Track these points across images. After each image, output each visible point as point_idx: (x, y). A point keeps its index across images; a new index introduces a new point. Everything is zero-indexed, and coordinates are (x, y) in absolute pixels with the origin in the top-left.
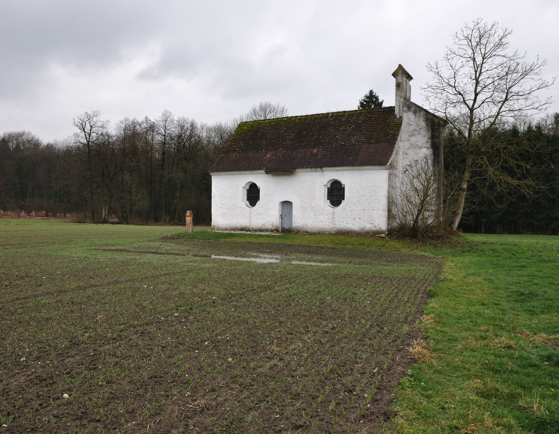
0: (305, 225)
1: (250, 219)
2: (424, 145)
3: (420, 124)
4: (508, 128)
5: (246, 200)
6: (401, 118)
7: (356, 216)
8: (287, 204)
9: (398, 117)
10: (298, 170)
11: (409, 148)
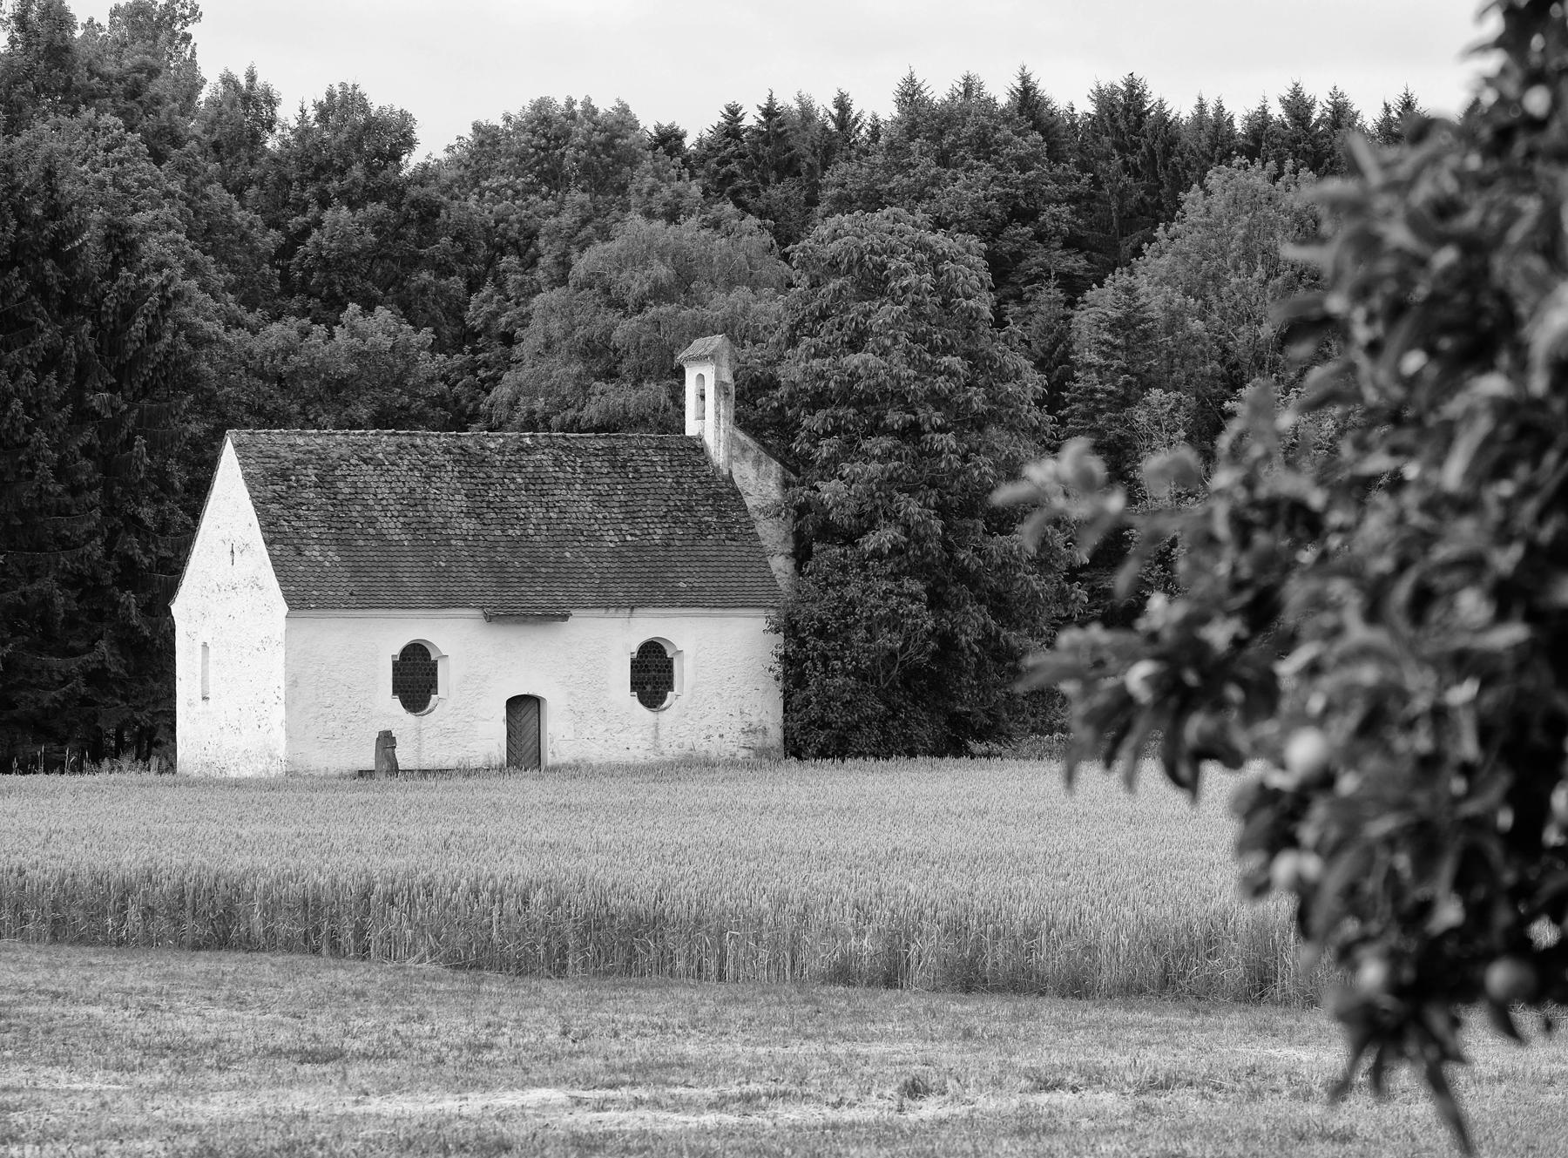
1: (419, 750)
2: (779, 548)
3: (1425, 908)
7: (711, 732)
8: (523, 709)
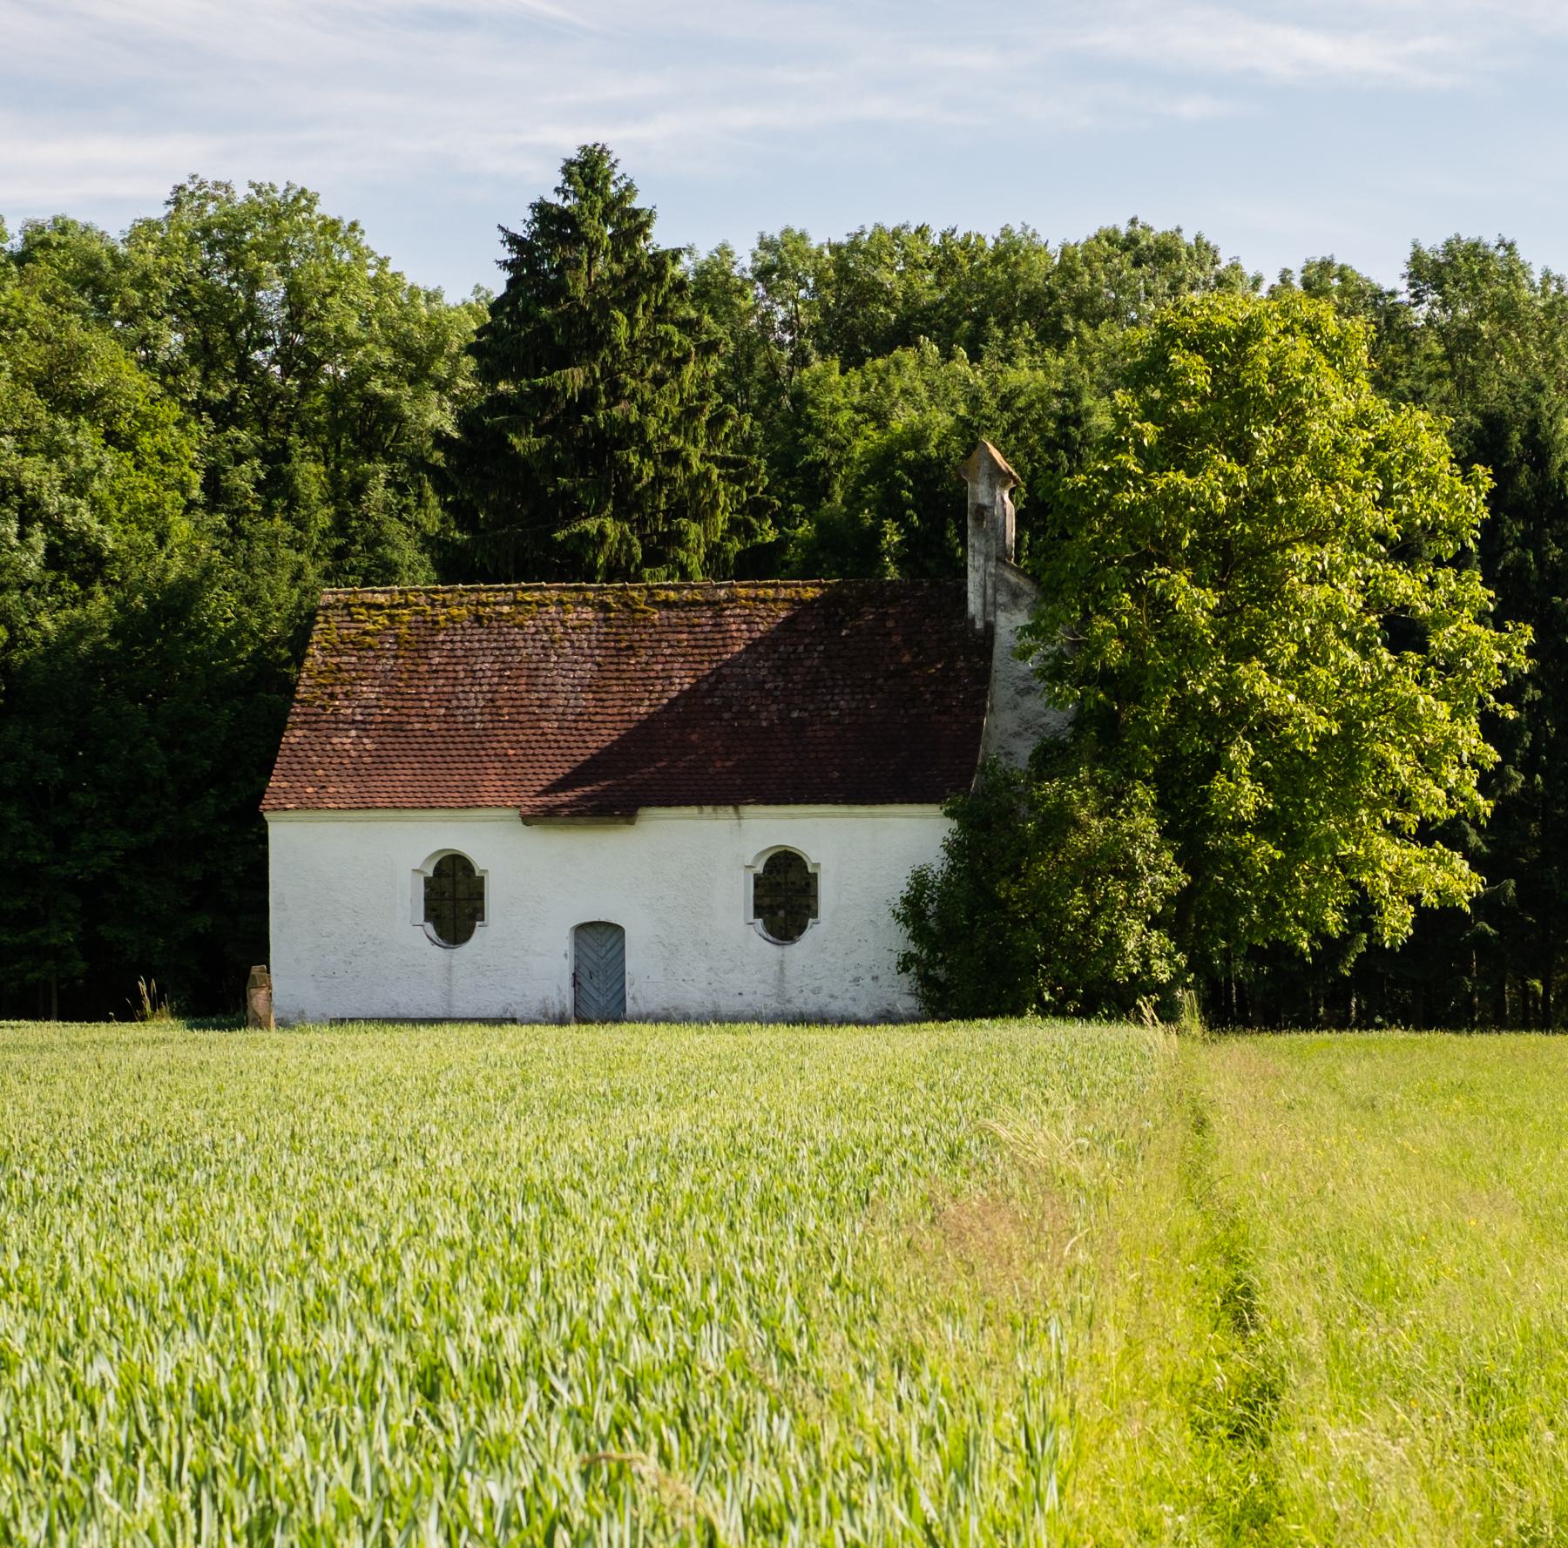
0: (676, 1009)
4: (1401, 939)
5: (422, 917)
6: (990, 628)
9: (979, 625)
10: (641, 811)
11: (1017, 735)
